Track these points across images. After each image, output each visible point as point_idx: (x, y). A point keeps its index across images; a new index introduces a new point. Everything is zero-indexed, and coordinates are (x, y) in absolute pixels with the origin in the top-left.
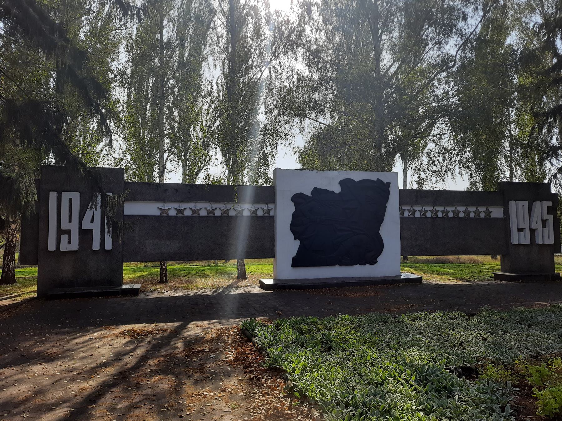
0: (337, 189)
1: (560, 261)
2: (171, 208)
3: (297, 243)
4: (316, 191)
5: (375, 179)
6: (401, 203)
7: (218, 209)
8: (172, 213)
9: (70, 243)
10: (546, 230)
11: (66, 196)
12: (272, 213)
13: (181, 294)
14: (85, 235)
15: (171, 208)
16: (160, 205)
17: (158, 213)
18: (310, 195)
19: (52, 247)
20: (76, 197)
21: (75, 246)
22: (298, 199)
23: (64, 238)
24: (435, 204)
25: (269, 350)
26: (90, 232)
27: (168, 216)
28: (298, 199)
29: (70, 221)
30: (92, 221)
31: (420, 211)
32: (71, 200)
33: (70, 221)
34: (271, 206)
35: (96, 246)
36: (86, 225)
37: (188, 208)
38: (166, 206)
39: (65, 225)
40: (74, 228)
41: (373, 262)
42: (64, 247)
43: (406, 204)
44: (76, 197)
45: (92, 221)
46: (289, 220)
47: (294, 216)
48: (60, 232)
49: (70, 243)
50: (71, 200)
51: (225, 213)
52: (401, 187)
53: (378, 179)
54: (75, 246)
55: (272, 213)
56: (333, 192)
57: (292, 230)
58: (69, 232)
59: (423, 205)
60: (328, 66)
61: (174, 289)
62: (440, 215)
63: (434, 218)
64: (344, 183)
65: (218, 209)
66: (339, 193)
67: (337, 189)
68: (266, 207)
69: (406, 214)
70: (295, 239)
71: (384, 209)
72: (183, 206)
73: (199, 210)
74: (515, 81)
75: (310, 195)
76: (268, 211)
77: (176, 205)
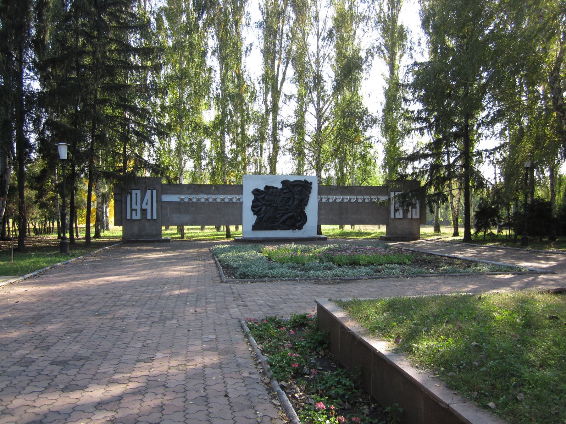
0: (280, 186)
2: (185, 197)
3: (255, 217)
6: (319, 193)
8: (186, 200)
9: (136, 215)
12: (241, 200)
14: (144, 211)
15: (185, 197)
19: (129, 217)
20: (139, 192)
21: (139, 217)
22: (256, 192)
23: (134, 213)
25: (315, 352)
26: (146, 210)
27: (184, 202)
28: (256, 192)
29: (136, 205)
30: (147, 204)
32: (136, 194)
33: (136, 205)
34: (240, 196)
35: (149, 217)
36: (144, 207)
38: (183, 197)
39: (134, 207)
40: (138, 208)
41: (300, 228)
42: (134, 217)
43: (323, 194)
44: (139, 192)
45: (147, 204)
46: (250, 204)
48: (132, 210)
49: (136, 215)
50: (136, 194)
52: (155, 192)
54: (139, 217)
55: (241, 200)
56: (277, 188)
57: (253, 211)
58: (136, 210)
59: (370, 195)
61: (194, 252)
62: (345, 201)
63: (342, 202)
67: (280, 186)
68: (238, 197)
69: (324, 200)
71: (308, 197)
72: (192, 196)
74: (56, 224)
76: (239, 199)
77: (188, 196)
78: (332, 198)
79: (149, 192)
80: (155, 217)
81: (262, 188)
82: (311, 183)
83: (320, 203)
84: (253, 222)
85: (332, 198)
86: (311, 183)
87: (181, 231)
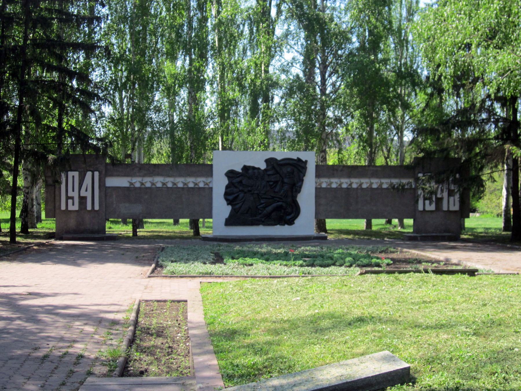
0: (263, 166)
1: (4, 212)
3: (230, 208)
4: (246, 168)
5: (296, 158)
7: (201, 181)
10: (452, 199)
11: (71, 174)
13: (127, 245)
14: (83, 200)
16: (129, 179)
17: (127, 185)
18: (240, 171)
19: (63, 208)
21: (76, 207)
22: (231, 174)
23: (70, 201)
24: (349, 176)
28: (231, 174)
30: (86, 190)
31: (357, 183)
32: (73, 177)
33: (73, 191)
34: (209, 180)
35: (89, 208)
37: (345, 183)
39: (70, 194)
40: (75, 195)
41: (291, 222)
42: (71, 208)
43: (324, 176)
44: (76, 174)
45: (86, 190)
47: (227, 187)
48: (68, 198)
49: (73, 204)
50: (73, 177)
51: (329, 185)
53: (298, 158)
54: (76, 207)
56: (259, 169)
58: (72, 198)
60: (111, 92)
64: (269, 161)
65: (201, 181)
66: (265, 170)
67: (263, 166)
70: (228, 204)
73: (189, 182)
75: (240, 171)
77: (139, 179)
78: (335, 182)
79: (89, 174)
80: (97, 208)
81: (239, 169)
82: (306, 161)
83: (319, 191)
84: (227, 215)
85: (335, 182)
86: (306, 161)
87: (369, 225)
